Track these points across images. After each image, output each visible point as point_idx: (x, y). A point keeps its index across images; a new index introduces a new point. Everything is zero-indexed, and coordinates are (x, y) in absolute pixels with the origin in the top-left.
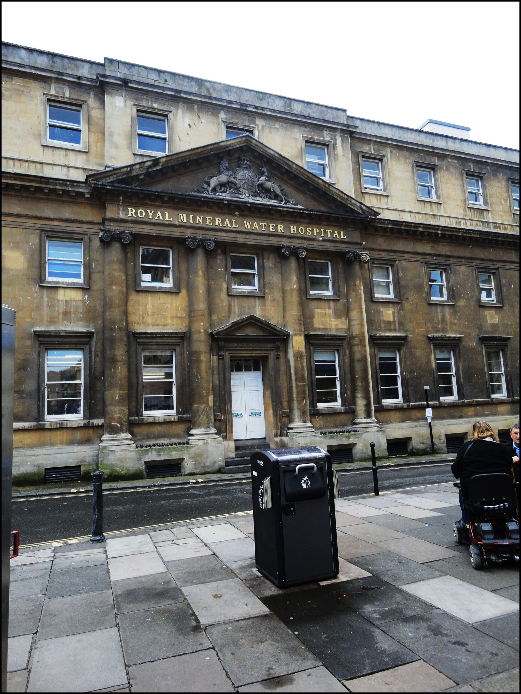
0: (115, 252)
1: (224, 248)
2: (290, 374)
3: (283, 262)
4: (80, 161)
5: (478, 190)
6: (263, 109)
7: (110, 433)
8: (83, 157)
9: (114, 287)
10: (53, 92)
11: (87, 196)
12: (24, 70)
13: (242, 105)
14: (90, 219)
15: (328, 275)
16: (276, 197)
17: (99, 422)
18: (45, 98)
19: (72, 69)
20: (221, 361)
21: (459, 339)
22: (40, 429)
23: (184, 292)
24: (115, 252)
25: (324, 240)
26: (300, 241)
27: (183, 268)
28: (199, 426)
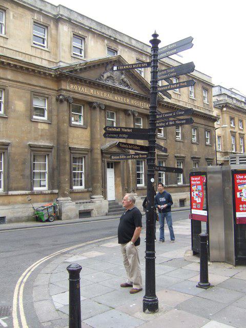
0: (65, 106)
1: (107, 107)
2: (129, 170)
3: (127, 117)
4: (46, 56)
5: (82, 47)
6: (122, 41)
7: (63, 197)
8: (47, 54)
9: (65, 124)
10: (36, 18)
11: (53, 76)
12: (25, 4)
13: (115, 38)
14: (52, 87)
15: (140, 124)
16: (127, 85)
17: (56, 191)
18: (32, 21)
19: (44, 7)
20: (103, 163)
21: (184, 157)
22: (33, 194)
23: (89, 128)
24: (65, 106)
25: (143, 108)
26: (135, 108)
27: (89, 116)
28: (97, 195)
